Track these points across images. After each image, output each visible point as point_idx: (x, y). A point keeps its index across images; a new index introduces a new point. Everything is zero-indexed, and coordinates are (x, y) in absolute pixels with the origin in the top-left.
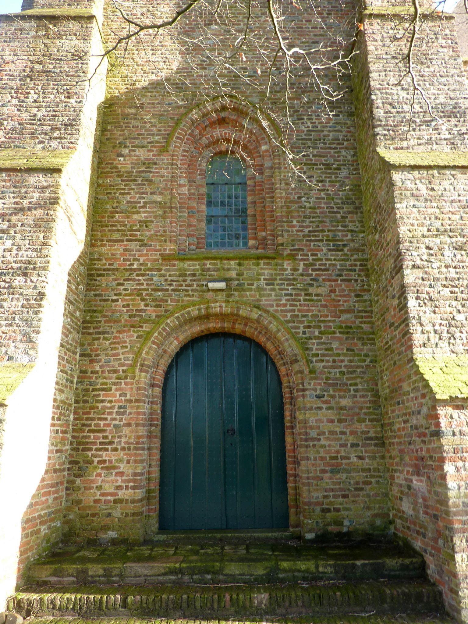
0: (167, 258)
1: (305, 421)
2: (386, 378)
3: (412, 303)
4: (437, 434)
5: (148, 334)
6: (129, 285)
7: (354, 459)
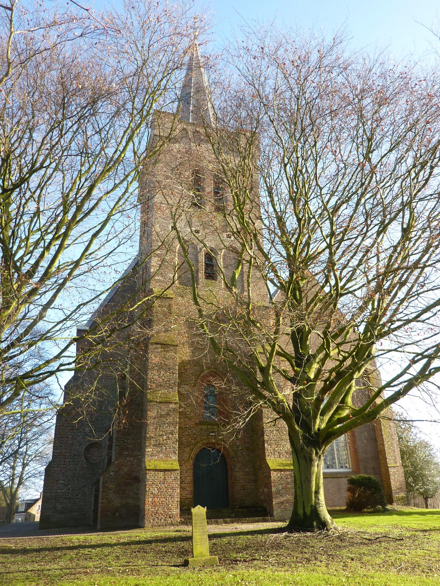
0: (196, 424)
1: (236, 475)
2: (258, 463)
3: (266, 445)
4: (270, 477)
5: (193, 449)
6: (186, 433)
7: (248, 486)
